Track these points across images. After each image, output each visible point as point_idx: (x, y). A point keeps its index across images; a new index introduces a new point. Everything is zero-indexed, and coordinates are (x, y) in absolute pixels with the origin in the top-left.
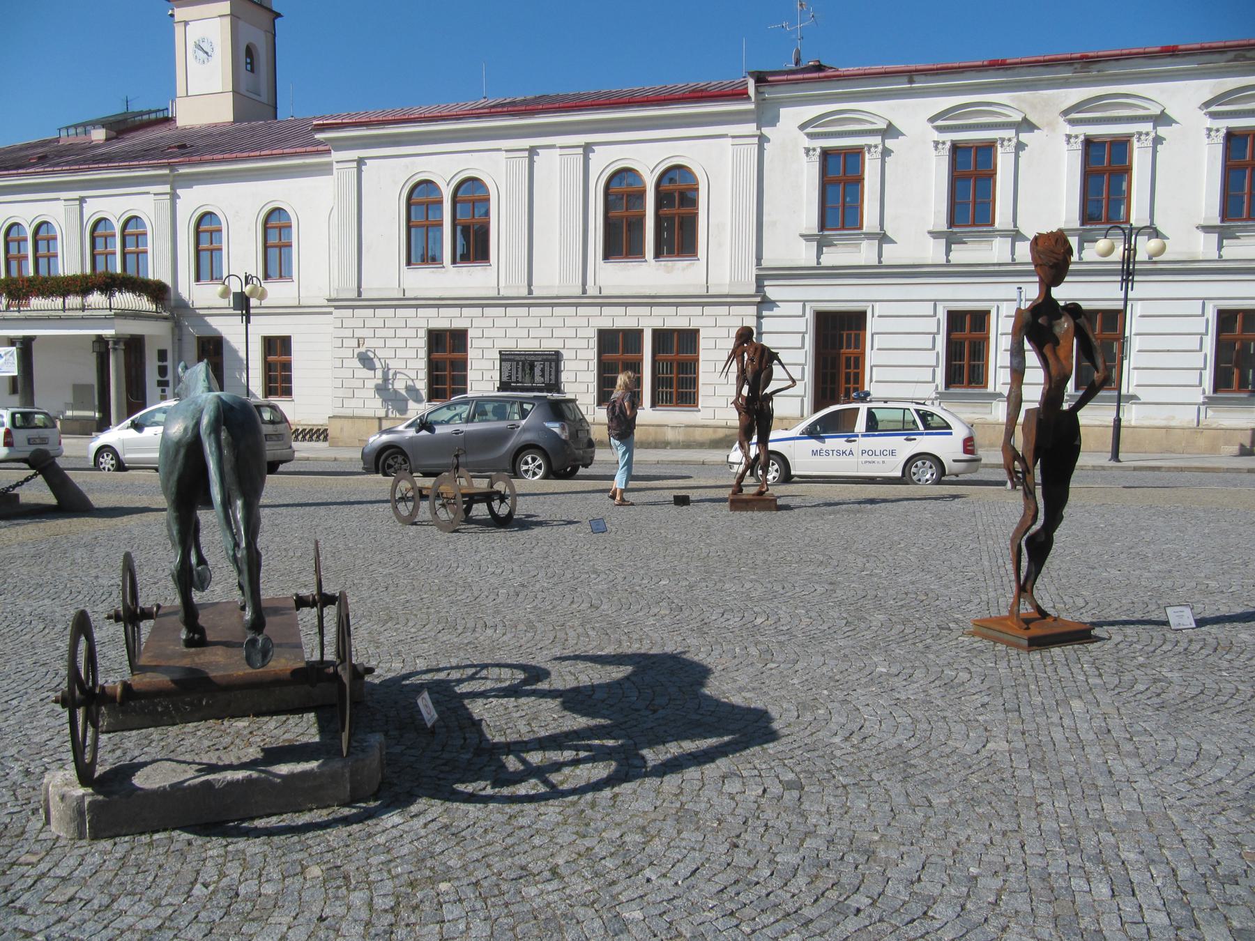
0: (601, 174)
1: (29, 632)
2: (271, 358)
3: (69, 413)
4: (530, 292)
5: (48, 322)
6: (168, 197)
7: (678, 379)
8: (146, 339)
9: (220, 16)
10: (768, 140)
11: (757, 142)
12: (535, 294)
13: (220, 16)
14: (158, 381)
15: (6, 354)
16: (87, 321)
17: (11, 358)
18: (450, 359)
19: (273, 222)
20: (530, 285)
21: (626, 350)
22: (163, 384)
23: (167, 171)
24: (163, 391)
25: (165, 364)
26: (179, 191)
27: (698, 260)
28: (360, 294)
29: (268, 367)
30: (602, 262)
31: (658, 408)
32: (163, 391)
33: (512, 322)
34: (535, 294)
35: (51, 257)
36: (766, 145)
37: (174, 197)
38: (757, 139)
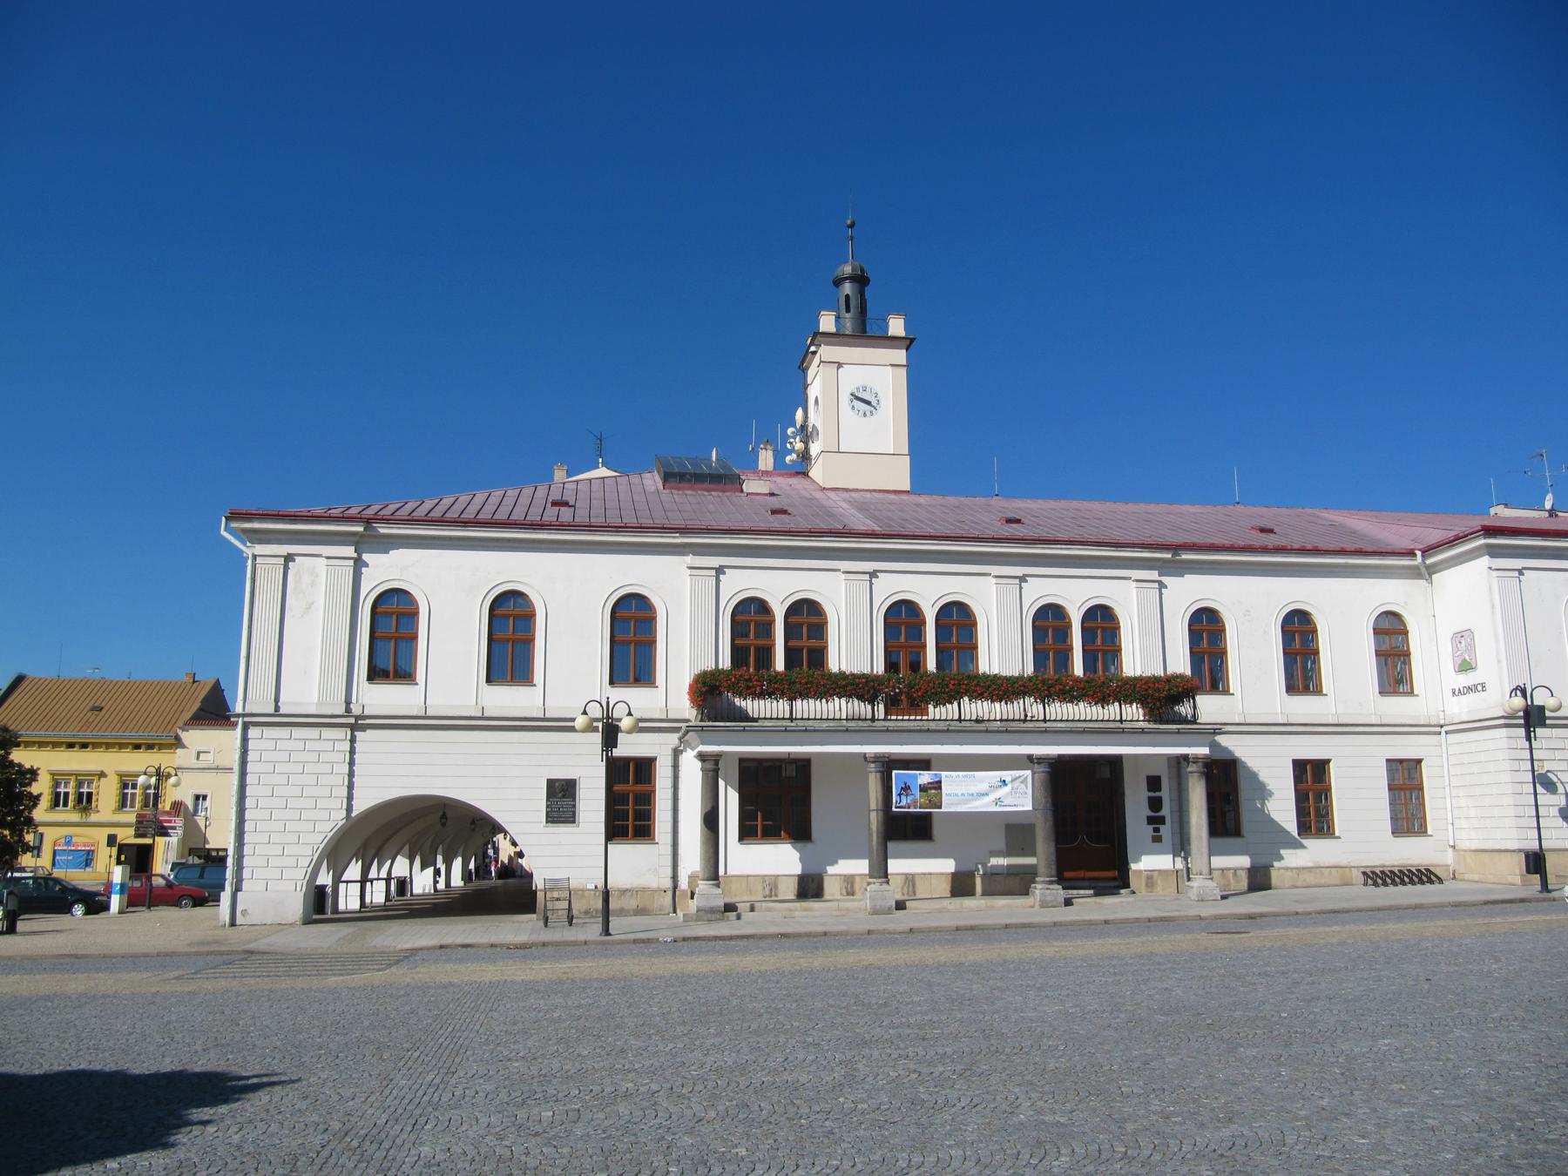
0: (939, 599)
1: (1433, 1159)
2: (617, 788)
3: (994, 861)
4: (277, 708)
5: (1045, 736)
6: (351, 563)
7: (636, 812)
8: (1124, 760)
9: (891, 365)
10: (1166, 587)
11: (352, 564)
12: (282, 711)
13: (891, 365)
14: (1148, 817)
15: (1013, 781)
16: (853, 735)
17: (1023, 786)
18: (633, 791)
19: (509, 607)
20: (277, 700)
21: (638, 781)
22: (1156, 821)
23: (361, 529)
24: (1156, 830)
25: (1157, 794)
26: (366, 557)
27: (535, 685)
28: (277, 708)
29: (1301, 797)
30: (366, 683)
31: (745, 842)
32: (1156, 830)
33: (271, 745)
34: (282, 711)
35: (1114, 652)
36: (364, 570)
37: (359, 564)
38: (352, 561)
